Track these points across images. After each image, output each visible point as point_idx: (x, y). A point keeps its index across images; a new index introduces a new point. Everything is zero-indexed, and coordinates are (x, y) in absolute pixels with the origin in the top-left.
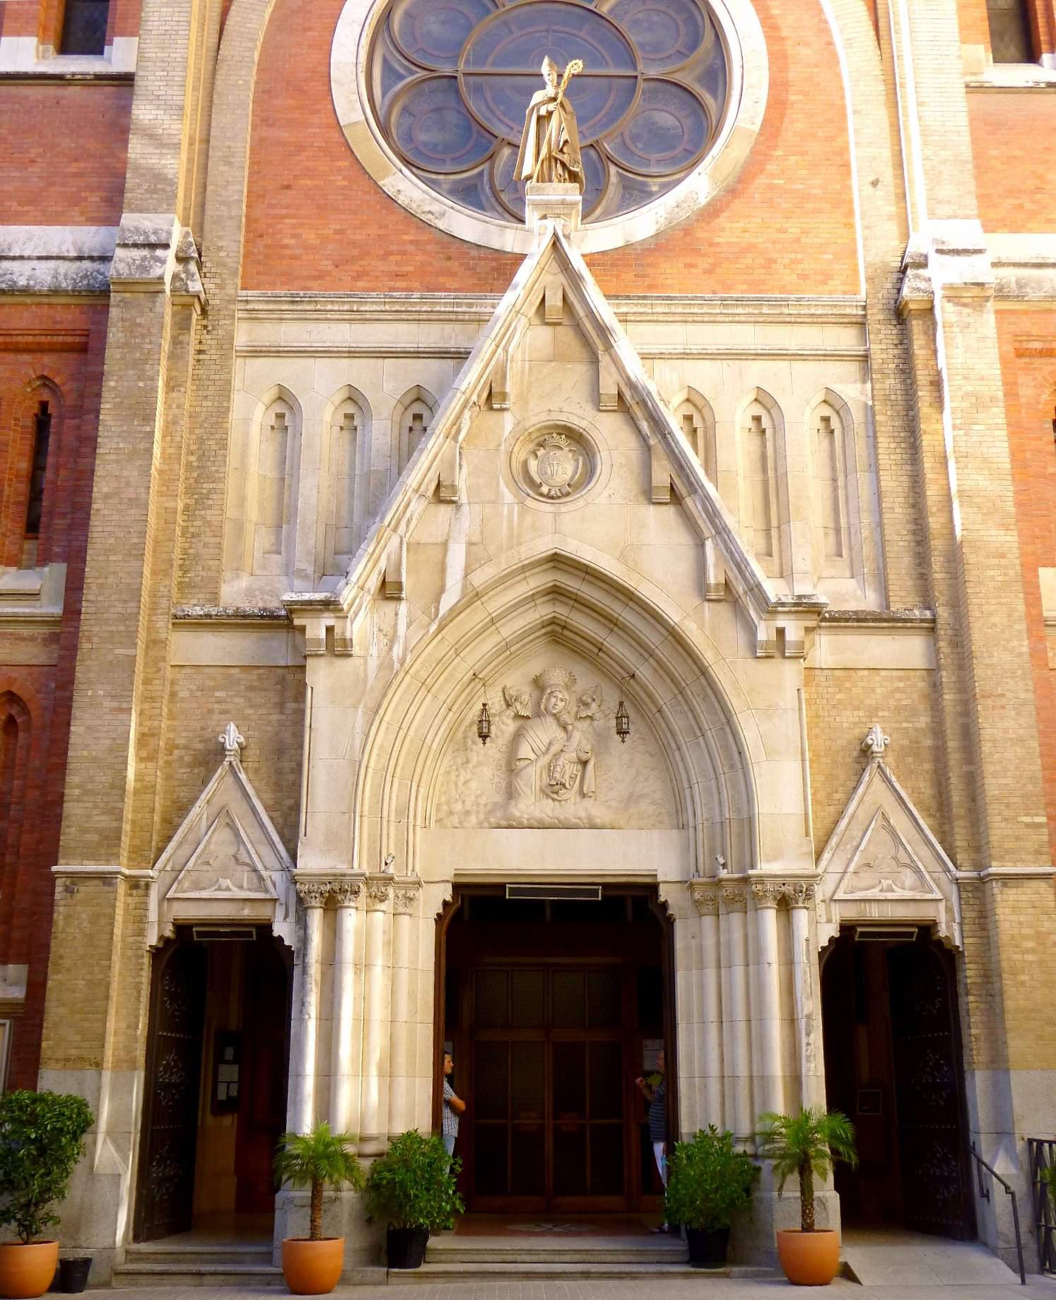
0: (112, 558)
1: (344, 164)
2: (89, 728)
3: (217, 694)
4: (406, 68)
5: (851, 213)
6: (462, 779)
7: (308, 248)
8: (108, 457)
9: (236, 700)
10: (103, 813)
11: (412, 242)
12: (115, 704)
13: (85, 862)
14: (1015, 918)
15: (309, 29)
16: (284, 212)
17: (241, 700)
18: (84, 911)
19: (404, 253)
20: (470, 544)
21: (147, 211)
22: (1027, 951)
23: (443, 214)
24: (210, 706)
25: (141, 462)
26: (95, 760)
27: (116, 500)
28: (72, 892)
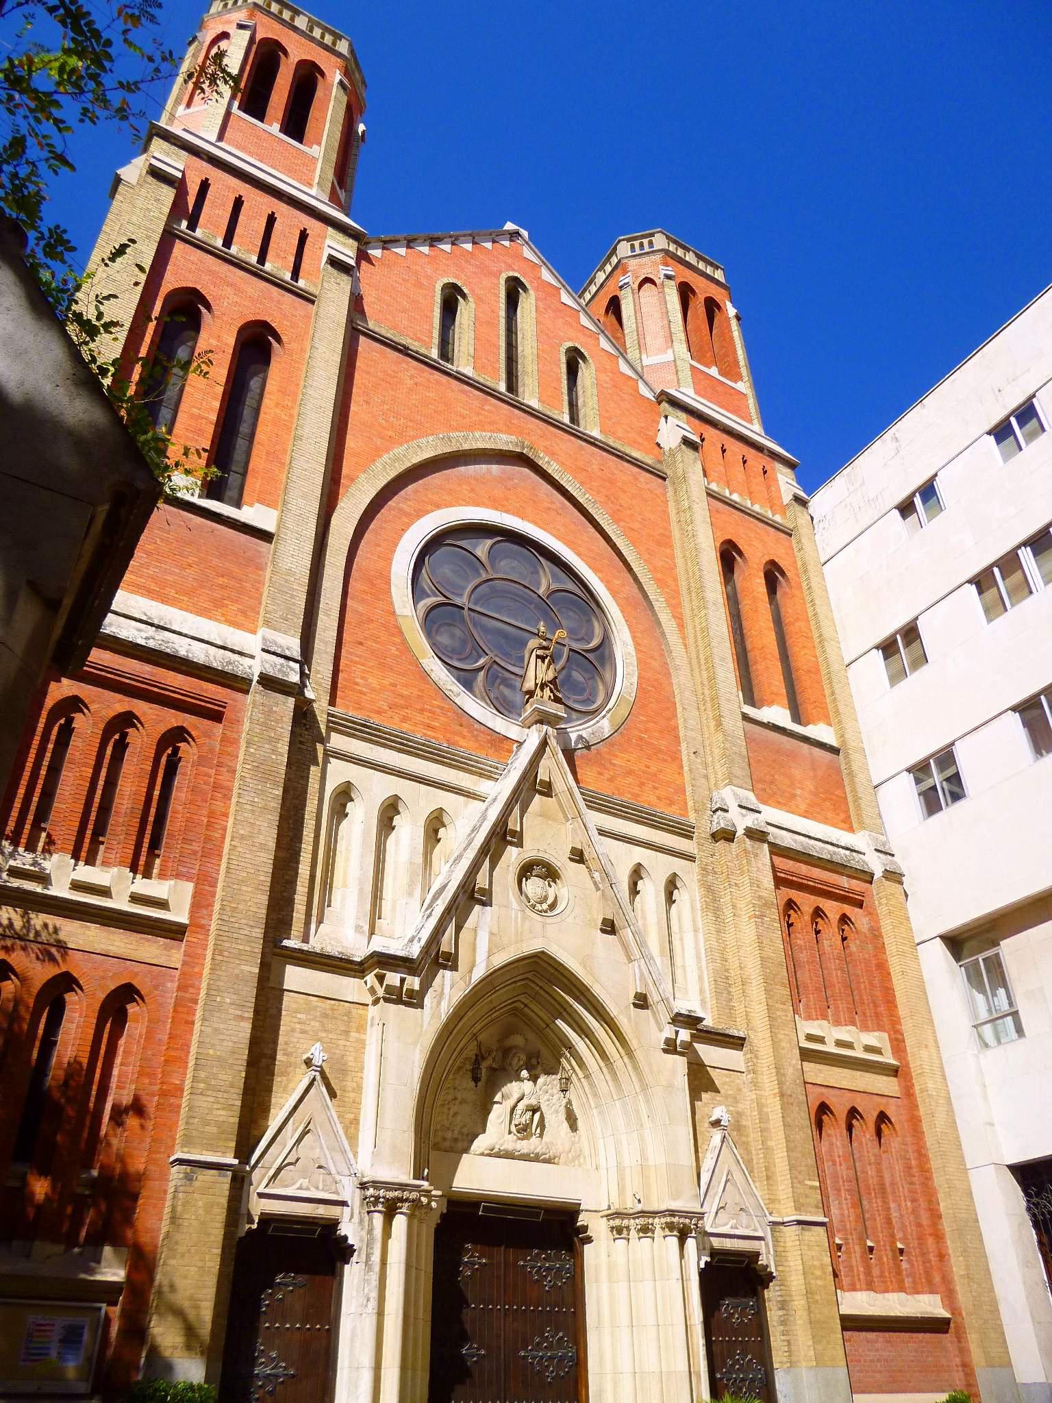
0: (244, 888)
1: (398, 640)
2: (216, 1030)
3: (299, 1016)
4: (432, 590)
5: (681, 767)
6: (451, 1113)
7: (373, 690)
8: (245, 806)
9: (313, 1023)
10: (223, 1109)
11: (438, 707)
12: (239, 1013)
13: (204, 1152)
14: (809, 1253)
15: (379, 546)
16: (357, 659)
17: (317, 1024)
18: (201, 1199)
19: (434, 713)
20: (491, 934)
21: (280, 631)
22: (817, 1278)
23: (459, 695)
24: (293, 1025)
25: (270, 817)
26: (219, 1059)
27: (249, 842)
28: (192, 1180)
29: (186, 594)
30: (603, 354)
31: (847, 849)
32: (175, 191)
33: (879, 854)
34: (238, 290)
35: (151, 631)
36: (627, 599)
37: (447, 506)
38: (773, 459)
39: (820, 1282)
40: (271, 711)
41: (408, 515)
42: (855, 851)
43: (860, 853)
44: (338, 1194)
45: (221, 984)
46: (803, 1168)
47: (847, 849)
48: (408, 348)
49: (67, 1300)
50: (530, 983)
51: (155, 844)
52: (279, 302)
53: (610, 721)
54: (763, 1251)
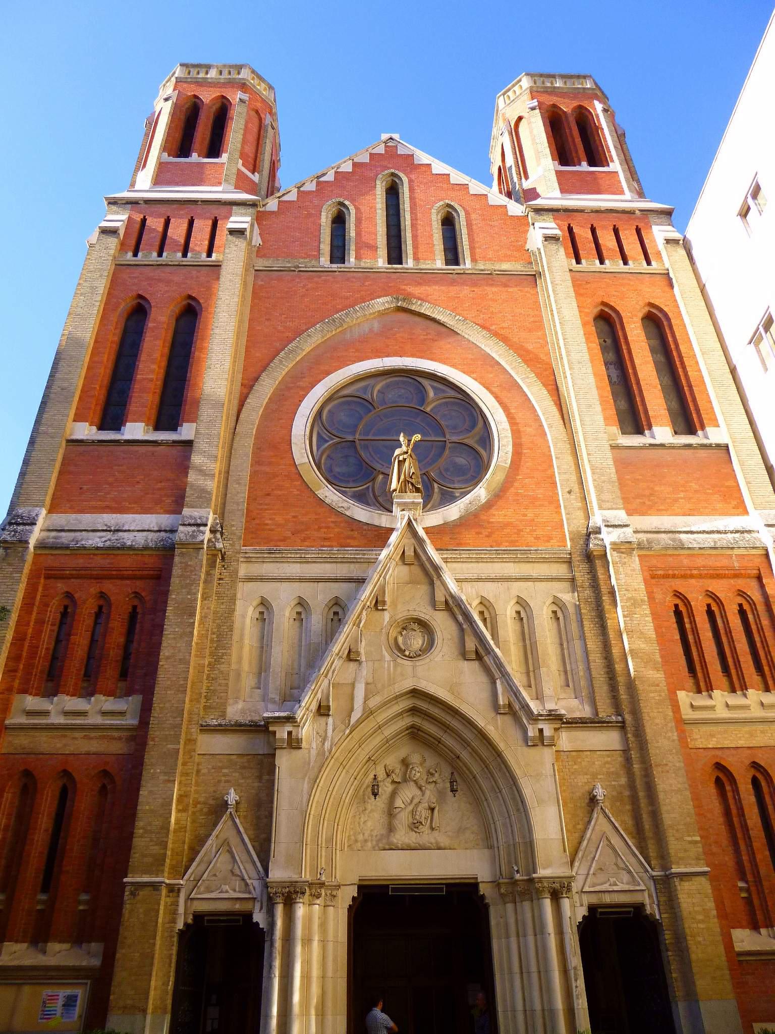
0: (169, 692)
8: (169, 636)
10: (156, 845)
11: (332, 522)
12: (166, 778)
14: (689, 900)
15: (281, 419)
16: (266, 507)
17: (237, 774)
20: (367, 684)
22: (699, 922)
26: (152, 811)
29: (135, 503)
30: (473, 197)
31: (737, 532)
32: (510, 214)
33: (770, 528)
34: (168, 282)
35: (109, 535)
36: (500, 386)
37: (336, 370)
39: (701, 926)
40: (187, 565)
41: (303, 389)
42: (747, 531)
43: (749, 532)
45: (152, 760)
46: (681, 827)
47: (737, 532)
49: (61, 979)
51: (678, 613)
52: (197, 277)
53: (486, 489)
54: (647, 901)
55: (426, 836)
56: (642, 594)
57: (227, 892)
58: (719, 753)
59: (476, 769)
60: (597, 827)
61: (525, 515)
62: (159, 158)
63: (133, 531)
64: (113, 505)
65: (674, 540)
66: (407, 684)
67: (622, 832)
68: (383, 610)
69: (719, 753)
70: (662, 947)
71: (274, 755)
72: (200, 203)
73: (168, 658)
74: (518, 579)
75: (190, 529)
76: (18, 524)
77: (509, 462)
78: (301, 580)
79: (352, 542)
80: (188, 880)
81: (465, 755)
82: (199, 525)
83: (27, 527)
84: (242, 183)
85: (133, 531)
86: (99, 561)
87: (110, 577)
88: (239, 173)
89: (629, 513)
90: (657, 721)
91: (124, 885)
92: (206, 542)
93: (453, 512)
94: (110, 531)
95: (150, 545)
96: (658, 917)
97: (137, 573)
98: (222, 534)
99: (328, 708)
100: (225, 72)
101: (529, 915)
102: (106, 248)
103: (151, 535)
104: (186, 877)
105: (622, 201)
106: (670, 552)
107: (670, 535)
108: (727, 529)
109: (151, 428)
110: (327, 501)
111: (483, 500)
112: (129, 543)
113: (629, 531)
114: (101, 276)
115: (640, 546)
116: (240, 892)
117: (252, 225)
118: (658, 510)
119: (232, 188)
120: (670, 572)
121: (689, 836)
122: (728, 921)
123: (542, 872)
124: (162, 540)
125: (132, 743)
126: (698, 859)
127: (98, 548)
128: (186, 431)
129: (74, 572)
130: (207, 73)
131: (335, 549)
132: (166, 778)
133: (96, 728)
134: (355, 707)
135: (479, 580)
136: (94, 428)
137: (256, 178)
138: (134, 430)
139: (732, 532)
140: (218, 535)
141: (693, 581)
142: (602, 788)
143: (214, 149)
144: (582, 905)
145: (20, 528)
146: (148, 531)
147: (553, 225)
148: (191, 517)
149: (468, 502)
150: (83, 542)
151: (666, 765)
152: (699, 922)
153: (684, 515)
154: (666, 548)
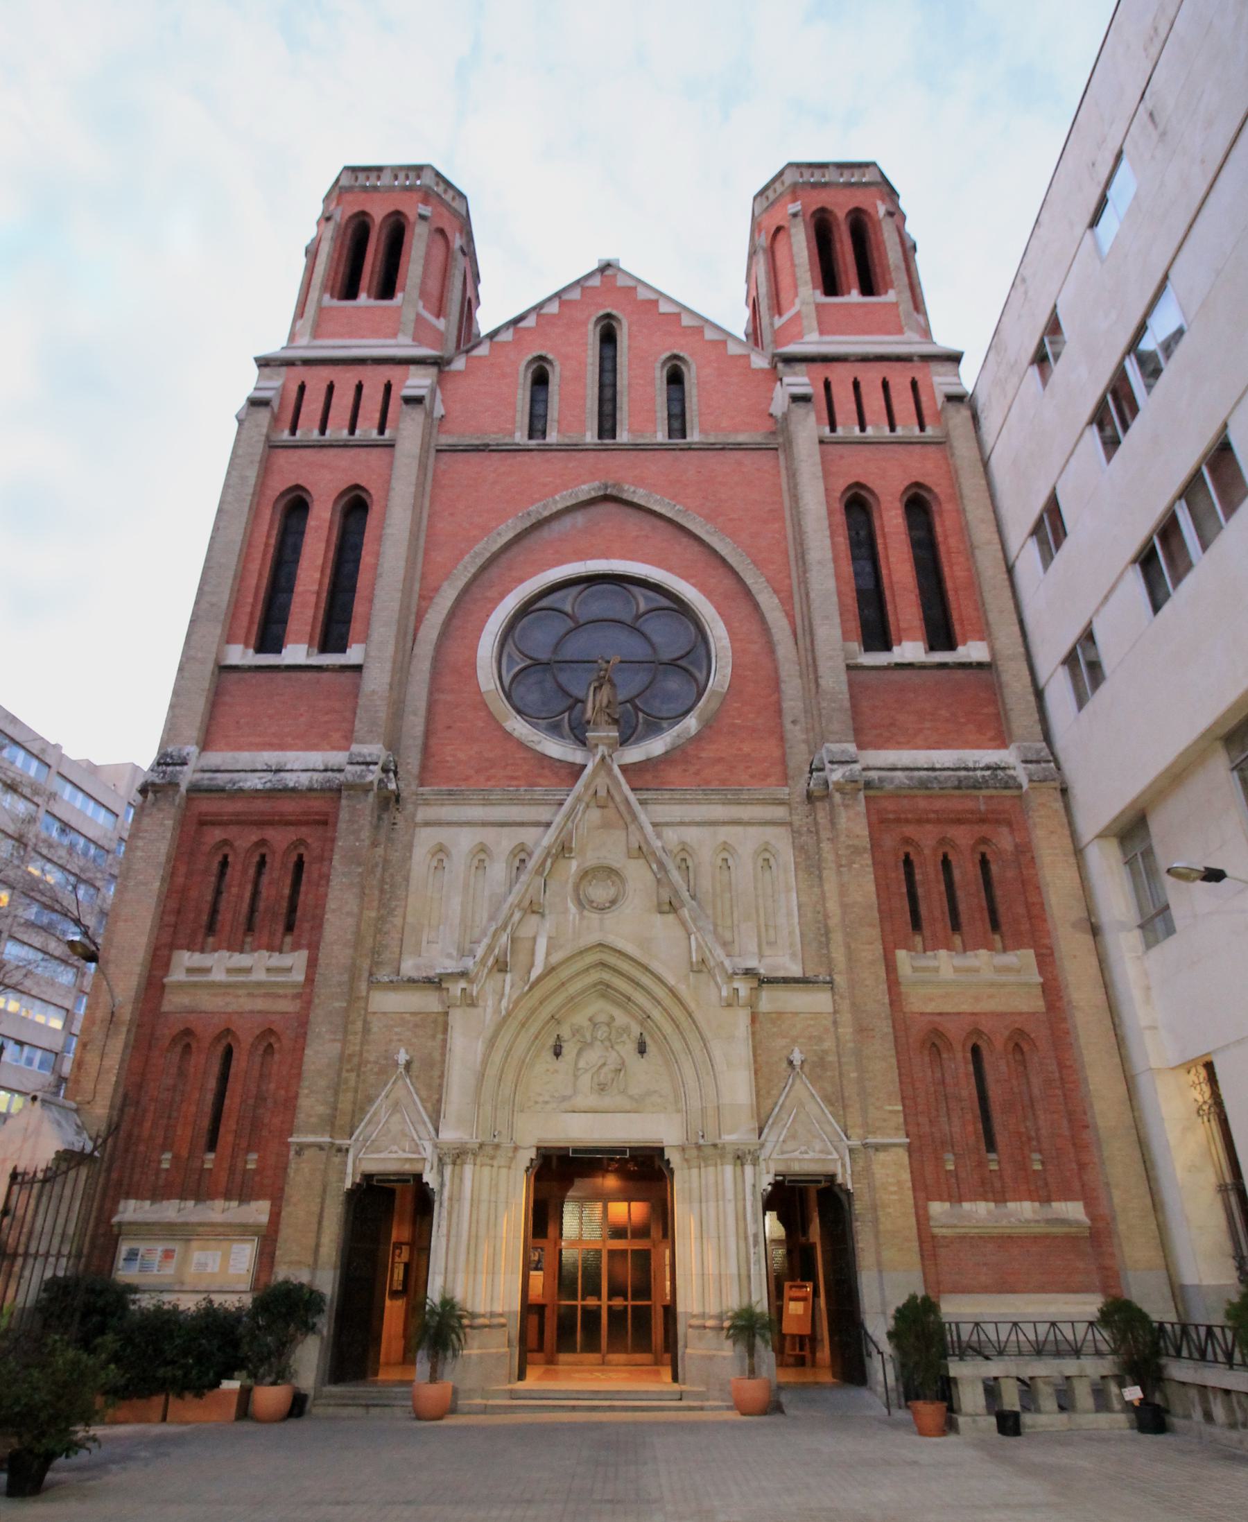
1: (482, 714)
12: (332, 1037)
20: (550, 938)
22: (892, 1193)
35: (269, 776)
37: (531, 577)
38: (927, 361)
39: (894, 1197)
44: (420, 1153)
48: (488, 445)
50: (606, 976)
54: (839, 1171)
55: (607, 1102)
56: (866, 843)
57: (396, 1152)
58: (937, 1019)
59: (668, 1028)
60: (792, 1094)
61: (740, 749)
62: (320, 301)
63: (296, 771)
64: (275, 741)
65: (911, 779)
66: (593, 938)
67: (819, 1099)
68: (569, 858)
69: (937, 1019)
70: (853, 1218)
71: (447, 1014)
72: (369, 362)
73: (334, 911)
74: (724, 823)
75: (358, 768)
76: (168, 765)
77: (726, 686)
78: (484, 824)
79: (541, 781)
80: (356, 1140)
81: (656, 1013)
82: (368, 764)
83: (178, 768)
84: (421, 330)
85: (296, 771)
86: (260, 805)
87: (271, 823)
88: (419, 319)
89: (861, 746)
90: (867, 983)
91: (288, 1145)
92: (376, 783)
93: (656, 746)
94: (271, 771)
95: (315, 786)
96: (850, 1187)
97: (301, 818)
98: (396, 773)
99: (506, 964)
100: (402, 175)
101: (711, 1179)
102: (257, 426)
103: (316, 776)
104: (354, 1138)
105: (897, 343)
106: (904, 792)
107: (907, 773)
108: (977, 766)
109: (316, 650)
110: (516, 734)
111: (693, 731)
112: (291, 784)
113: (857, 767)
114: (252, 462)
115: (868, 785)
116: (409, 1152)
117: (433, 392)
118: (898, 743)
119: (408, 341)
120: (903, 816)
121: (890, 1105)
122: (924, 1189)
123: (727, 1138)
124: (329, 781)
125: (298, 1001)
126: (897, 1129)
127: (257, 791)
128: (354, 654)
129: (233, 818)
130: (379, 178)
131: (522, 789)
132: (332, 1037)
133: (259, 984)
134: (536, 963)
135: (682, 824)
136: (251, 651)
137: (441, 324)
138: (296, 653)
139: (982, 769)
140: (391, 775)
141: (929, 827)
142: (801, 1052)
143: (387, 289)
144: (768, 1173)
145: (170, 769)
146: (314, 770)
147: (805, 380)
148: (360, 755)
149: (675, 734)
150: (241, 784)
151: (873, 1030)
152: (892, 1193)
153: (929, 748)
154: (900, 788)
